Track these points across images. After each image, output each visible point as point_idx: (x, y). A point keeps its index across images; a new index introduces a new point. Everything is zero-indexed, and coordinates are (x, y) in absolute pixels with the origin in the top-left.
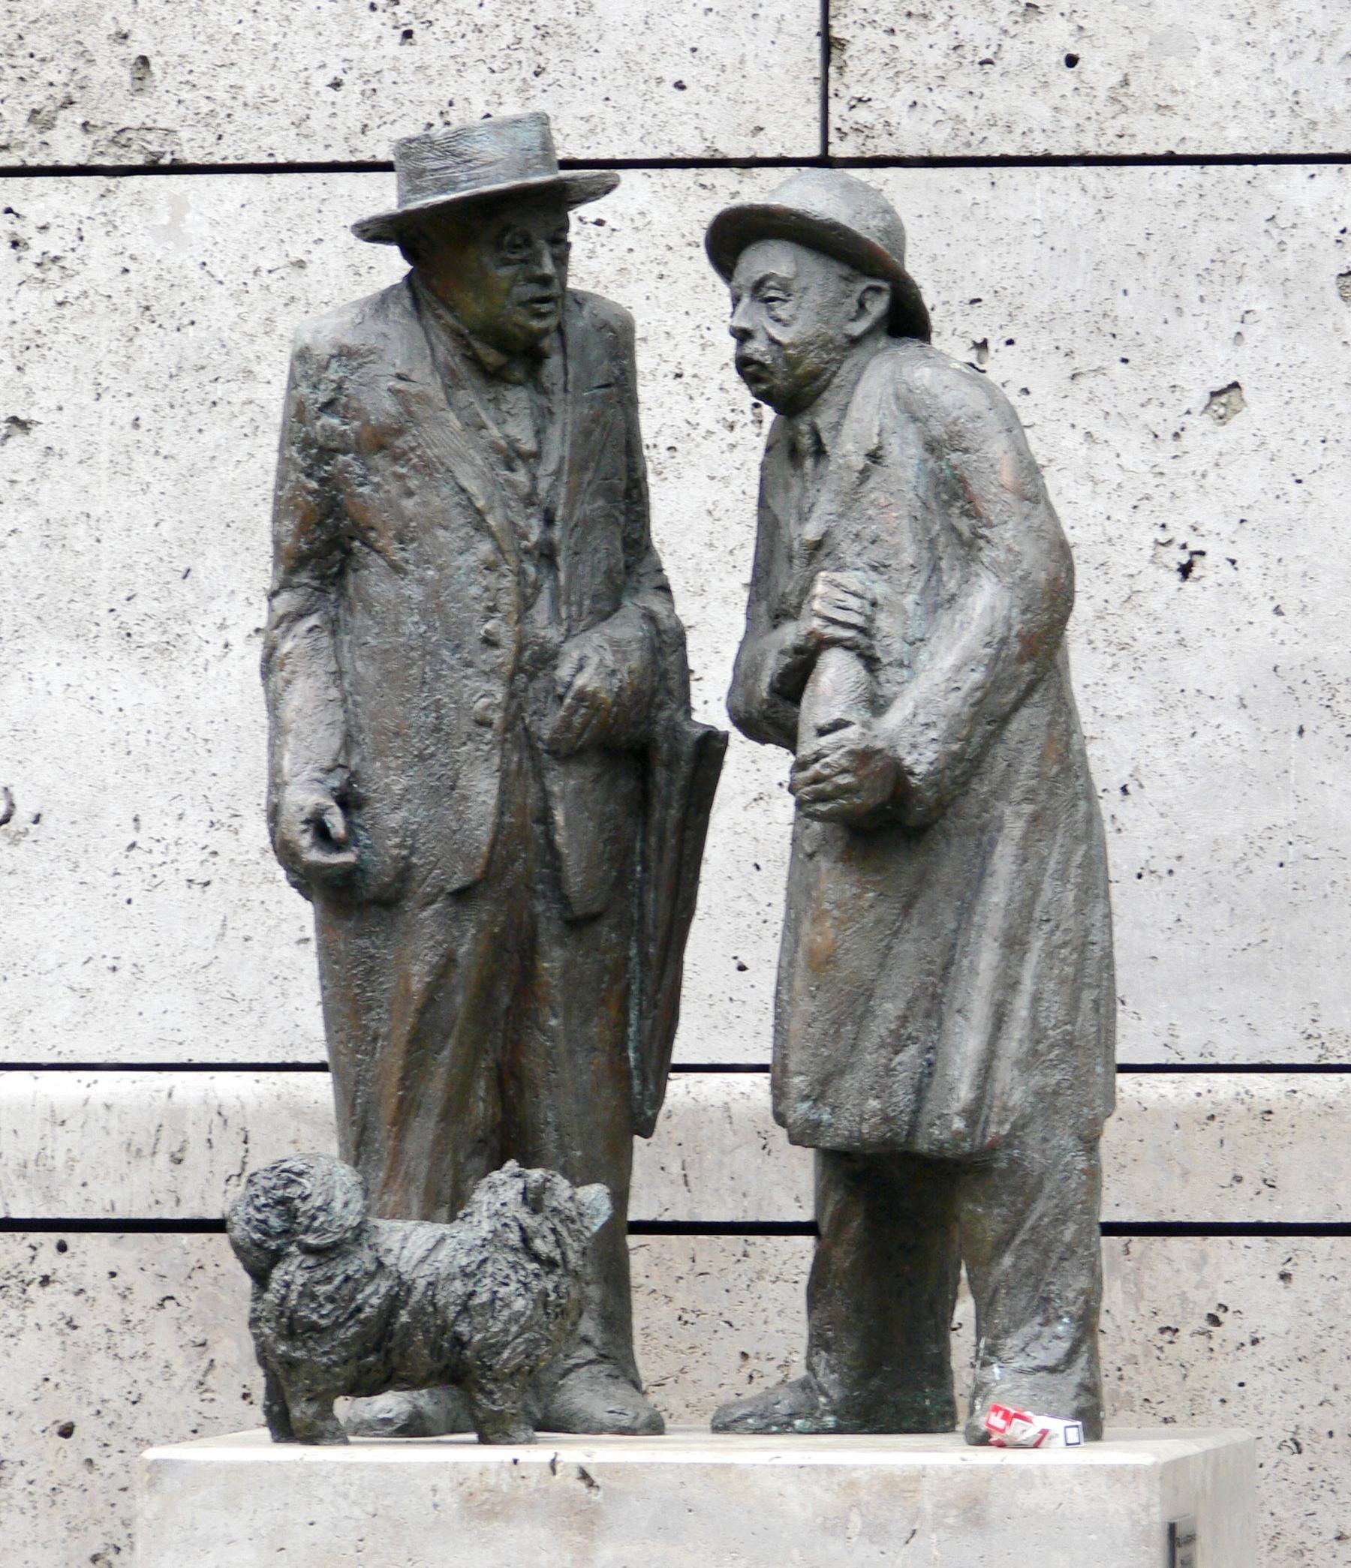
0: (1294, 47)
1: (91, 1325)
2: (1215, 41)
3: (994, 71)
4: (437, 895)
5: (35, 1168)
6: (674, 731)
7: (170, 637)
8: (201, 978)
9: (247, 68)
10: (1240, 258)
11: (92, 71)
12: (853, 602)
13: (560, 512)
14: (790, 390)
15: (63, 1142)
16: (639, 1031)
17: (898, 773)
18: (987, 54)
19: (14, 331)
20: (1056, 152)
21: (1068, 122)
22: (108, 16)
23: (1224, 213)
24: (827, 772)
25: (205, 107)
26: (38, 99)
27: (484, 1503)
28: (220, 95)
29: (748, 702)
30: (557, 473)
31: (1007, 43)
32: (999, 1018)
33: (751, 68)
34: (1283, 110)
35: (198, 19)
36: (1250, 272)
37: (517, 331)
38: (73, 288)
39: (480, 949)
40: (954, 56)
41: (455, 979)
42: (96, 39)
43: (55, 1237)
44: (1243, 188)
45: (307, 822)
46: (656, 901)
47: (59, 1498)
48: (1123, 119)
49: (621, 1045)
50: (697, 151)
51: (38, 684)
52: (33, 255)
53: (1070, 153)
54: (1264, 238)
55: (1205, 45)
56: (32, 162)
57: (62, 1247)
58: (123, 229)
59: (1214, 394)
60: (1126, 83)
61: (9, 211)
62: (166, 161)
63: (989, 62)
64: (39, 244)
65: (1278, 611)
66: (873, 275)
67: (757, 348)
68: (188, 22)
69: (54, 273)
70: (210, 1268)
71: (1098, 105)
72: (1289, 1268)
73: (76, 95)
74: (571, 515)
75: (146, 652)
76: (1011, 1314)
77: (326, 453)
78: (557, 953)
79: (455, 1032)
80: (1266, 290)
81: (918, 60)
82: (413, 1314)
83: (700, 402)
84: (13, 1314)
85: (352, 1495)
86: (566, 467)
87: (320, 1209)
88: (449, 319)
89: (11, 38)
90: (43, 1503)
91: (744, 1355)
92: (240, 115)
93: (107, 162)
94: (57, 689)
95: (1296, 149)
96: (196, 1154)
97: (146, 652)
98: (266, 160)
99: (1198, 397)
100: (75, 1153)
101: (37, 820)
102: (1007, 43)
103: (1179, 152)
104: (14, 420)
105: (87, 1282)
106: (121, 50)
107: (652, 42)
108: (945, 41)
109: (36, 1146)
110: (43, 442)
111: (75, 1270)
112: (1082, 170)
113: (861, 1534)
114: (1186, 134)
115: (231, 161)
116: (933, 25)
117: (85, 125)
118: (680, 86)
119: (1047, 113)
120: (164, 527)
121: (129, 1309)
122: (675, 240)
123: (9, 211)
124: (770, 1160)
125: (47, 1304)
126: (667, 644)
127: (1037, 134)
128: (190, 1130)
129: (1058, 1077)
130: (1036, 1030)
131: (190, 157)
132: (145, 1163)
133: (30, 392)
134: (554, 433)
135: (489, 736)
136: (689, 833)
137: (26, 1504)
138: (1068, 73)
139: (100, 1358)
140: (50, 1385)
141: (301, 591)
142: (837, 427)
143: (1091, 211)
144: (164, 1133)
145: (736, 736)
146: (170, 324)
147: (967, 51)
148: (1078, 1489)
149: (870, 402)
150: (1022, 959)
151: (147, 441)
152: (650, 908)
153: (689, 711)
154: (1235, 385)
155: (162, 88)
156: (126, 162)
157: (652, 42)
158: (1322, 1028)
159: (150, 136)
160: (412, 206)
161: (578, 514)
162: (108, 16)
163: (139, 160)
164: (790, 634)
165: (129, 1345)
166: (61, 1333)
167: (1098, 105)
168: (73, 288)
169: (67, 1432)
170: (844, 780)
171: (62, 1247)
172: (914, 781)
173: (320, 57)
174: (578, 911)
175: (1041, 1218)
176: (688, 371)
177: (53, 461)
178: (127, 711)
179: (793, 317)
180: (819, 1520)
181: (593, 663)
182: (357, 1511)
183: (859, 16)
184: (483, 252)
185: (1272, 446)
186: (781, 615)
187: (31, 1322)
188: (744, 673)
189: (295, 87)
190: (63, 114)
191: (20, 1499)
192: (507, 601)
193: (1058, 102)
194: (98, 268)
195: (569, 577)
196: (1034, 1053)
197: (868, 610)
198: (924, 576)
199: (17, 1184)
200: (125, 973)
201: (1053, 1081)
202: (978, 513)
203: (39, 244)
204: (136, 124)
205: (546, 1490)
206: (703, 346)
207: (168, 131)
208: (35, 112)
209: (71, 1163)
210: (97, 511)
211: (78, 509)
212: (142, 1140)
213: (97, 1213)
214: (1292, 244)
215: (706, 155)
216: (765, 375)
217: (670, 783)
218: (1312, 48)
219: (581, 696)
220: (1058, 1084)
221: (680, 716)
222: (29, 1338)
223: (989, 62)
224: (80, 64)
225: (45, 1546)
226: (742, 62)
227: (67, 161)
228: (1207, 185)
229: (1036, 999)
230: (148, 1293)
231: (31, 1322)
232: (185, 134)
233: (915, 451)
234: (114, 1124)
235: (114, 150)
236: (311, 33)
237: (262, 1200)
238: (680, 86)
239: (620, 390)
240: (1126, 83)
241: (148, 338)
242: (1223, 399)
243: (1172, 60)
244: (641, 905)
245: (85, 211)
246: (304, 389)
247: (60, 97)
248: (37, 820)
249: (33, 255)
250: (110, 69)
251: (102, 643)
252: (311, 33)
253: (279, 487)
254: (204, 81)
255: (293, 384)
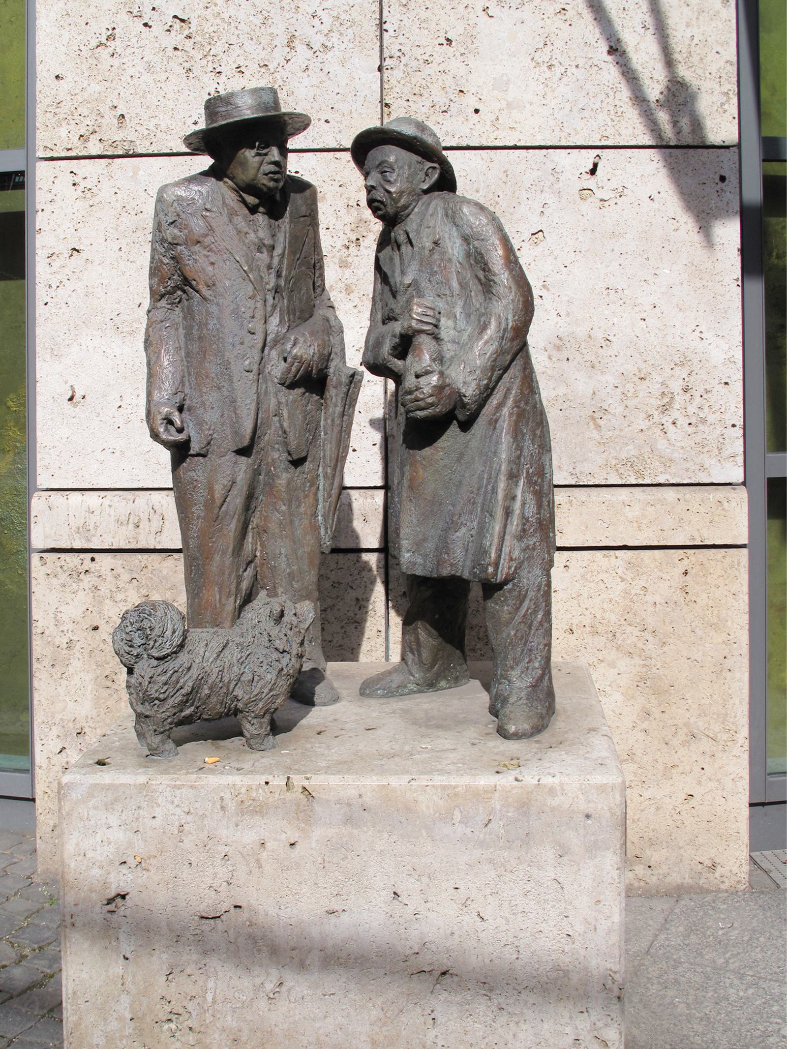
0: (561, 106)
1: (104, 589)
2: (531, 104)
3: (447, 115)
4: (226, 453)
5: (84, 530)
6: (338, 370)
7: (134, 329)
8: (147, 456)
9: (162, 118)
10: (542, 183)
11: (103, 121)
12: (430, 312)
13: (284, 273)
14: (390, 215)
15: (93, 519)
16: (324, 507)
17: (461, 396)
18: (445, 109)
19: (74, 217)
20: (472, 144)
21: (476, 134)
22: (109, 100)
23: (535, 167)
24: (422, 396)
25: (146, 132)
26: (82, 132)
27: (250, 806)
28: (151, 127)
29: (375, 358)
30: (282, 256)
31: (452, 104)
32: (508, 513)
33: (355, 115)
34: (557, 129)
35: (143, 100)
36: (546, 189)
37: (262, 187)
38: (96, 200)
39: (248, 477)
40: (432, 109)
41: (234, 491)
42: (105, 109)
43: (90, 555)
44: (542, 158)
45: (164, 419)
46: (331, 449)
47: (93, 654)
48: (496, 133)
49: (315, 515)
50: (334, 145)
51: (84, 347)
52: (81, 188)
53: (477, 145)
54: (551, 177)
55: (527, 105)
56: (80, 154)
57: (93, 559)
58: (115, 178)
59: (533, 234)
60: (497, 119)
61: (72, 172)
62: (131, 152)
63: (445, 111)
64: (83, 184)
65: (559, 315)
66: (433, 162)
67: (379, 195)
68: (139, 102)
69: (89, 195)
70: (150, 568)
71: (487, 127)
72: (568, 564)
73: (97, 129)
74: (290, 273)
75: (125, 334)
76: (514, 659)
77: (174, 245)
78: (285, 476)
79: (236, 516)
80: (552, 195)
81: (418, 111)
82: (211, 688)
83: (336, 238)
84: (74, 585)
85: (176, 803)
86: (287, 252)
87: (159, 636)
88: (230, 182)
89: (73, 109)
90: (86, 656)
91: (357, 599)
92: (159, 135)
93: (109, 153)
94: (91, 350)
95: (563, 144)
96: (144, 524)
97: (125, 334)
98: (169, 151)
99: (527, 235)
100: (98, 524)
101: (84, 397)
102: (452, 104)
103: (518, 144)
104: (74, 249)
105: (103, 572)
106: (114, 113)
107: (316, 106)
108: (428, 104)
109: (83, 521)
110: (85, 257)
111: (98, 568)
112: (481, 151)
113: (460, 822)
114: (521, 138)
115: (156, 152)
116: (424, 98)
117: (100, 140)
118: (327, 121)
119: (468, 131)
120: (131, 288)
121: (119, 583)
122: (326, 178)
123: (72, 172)
124: (367, 524)
125: (87, 581)
126: (332, 330)
127: (464, 138)
128: (141, 515)
129: (535, 540)
130: (524, 519)
131: (140, 151)
132: (124, 528)
133: (80, 239)
134: (281, 237)
135: (251, 377)
136: (345, 418)
137: (81, 657)
138: (475, 116)
139: (107, 601)
140: (89, 612)
141: (162, 310)
142: (418, 232)
143: (485, 167)
144: (131, 516)
145: (368, 376)
146: (133, 213)
147: (437, 107)
148: (581, 796)
149: (428, 221)
150: (517, 485)
151: (124, 256)
152: (328, 453)
153: (345, 362)
154: (541, 231)
155: (129, 126)
156: (116, 153)
157: (316, 106)
158: (577, 471)
159: (125, 144)
160: (210, 126)
161: (293, 273)
162: (109, 100)
163: (121, 153)
164: (397, 327)
165: (120, 596)
166: (92, 592)
167: (487, 127)
168: (96, 200)
169: (96, 628)
170: (430, 400)
171: (93, 559)
172: (466, 400)
173: (189, 113)
174: (295, 457)
175: (527, 611)
176: (331, 227)
177: (89, 265)
178: (118, 356)
179: (396, 180)
180: (437, 815)
181: (304, 348)
182: (178, 811)
183: (396, 95)
184: (243, 143)
185: (555, 254)
186: (389, 318)
187: (81, 588)
188: (372, 345)
189: (180, 124)
190: (92, 136)
191: (78, 655)
192: (259, 314)
193: (472, 126)
194: (105, 192)
195: (289, 301)
196: (524, 530)
197: (437, 316)
198: (463, 299)
199: (76, 536)
200: (117, 454)
201: (532, 543)
202: (489, 269)
203: (83, 184)
204: (120, 139)
205: (284, 799)
206: (337, 218)
207: (132, 142)
208: (81, 136)
209: (96, 527)
210: (105, 282)
211: (98, 282)
212: (123, 518)
213: (106, 546)
214: (562, 178)
215: (337, 147)
216: (382, 207)
217: (337, 395)
218: (568, 106)
219: (295, 358)
220: (534, 544)
221: (341, 365)
222: (81, 594)
223: (445, 111)
224: (98, 118)
225: (88, 672)
226: (351, 113)
227: (94, 153)
228: (529, 157)
229: (524, 504)
230: (126, 577)
231: (81, 588)
232: (138, 142)
233: (458, 242)
234: (112, 513)
235: (111, 148)
236: (186, 104)
237: (130, 629)
238: (327, 121)
239: (311, 218)
240: (497, 119)
241: (125, 218)
242: (536, 236)
243: (515, 111)
244: (324, 451)
245: (100, 172)
246: (161, 216)
247: (91, 130)
248: (84, 397)
249: (81, 188)
250: (110, 119)
251: (107, 331)
252: (186, 104)
253: (152, 262)
254: (145, 123)
255: (157, 214)
